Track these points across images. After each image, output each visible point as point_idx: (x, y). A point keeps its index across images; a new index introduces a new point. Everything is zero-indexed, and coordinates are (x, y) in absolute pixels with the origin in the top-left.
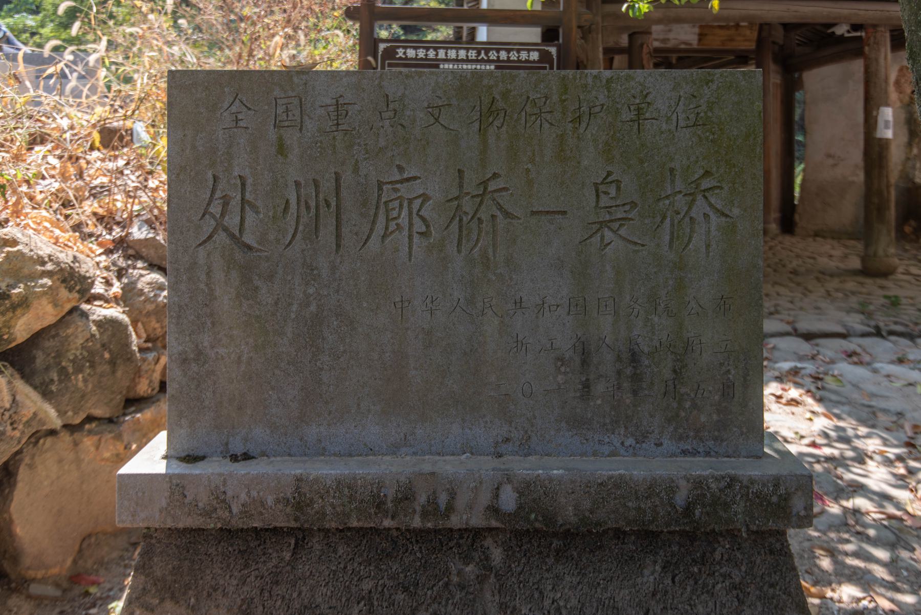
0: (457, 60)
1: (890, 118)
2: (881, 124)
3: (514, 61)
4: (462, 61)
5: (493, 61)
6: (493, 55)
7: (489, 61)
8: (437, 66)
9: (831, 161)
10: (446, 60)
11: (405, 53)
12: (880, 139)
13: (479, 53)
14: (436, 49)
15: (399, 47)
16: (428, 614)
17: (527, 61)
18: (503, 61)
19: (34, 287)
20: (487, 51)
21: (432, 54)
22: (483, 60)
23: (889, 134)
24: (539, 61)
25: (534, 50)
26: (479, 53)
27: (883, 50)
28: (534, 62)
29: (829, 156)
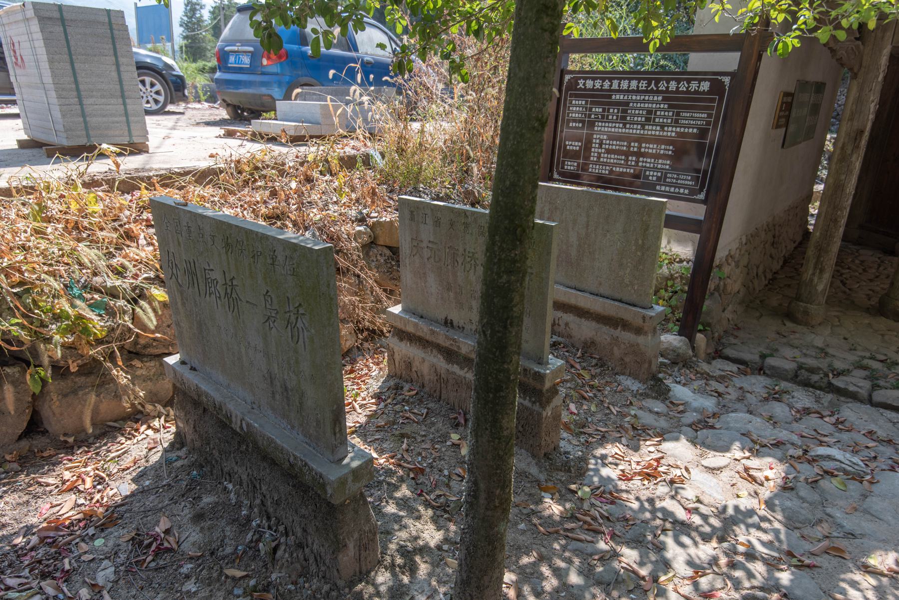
0: (628, 91)
3: (683, 92)
4: (633, 91)
7: (658, 92)
8: (610, 97)
10: (619, 91)
11: (584, 84)
13: (649, 84)
14: (611, 80)
15: (580, 78)
17: (696, 92)
18: (672, 92)
22: (652, 91)
25: (705, 80)
26: (649, 84)
28: (704, 93)
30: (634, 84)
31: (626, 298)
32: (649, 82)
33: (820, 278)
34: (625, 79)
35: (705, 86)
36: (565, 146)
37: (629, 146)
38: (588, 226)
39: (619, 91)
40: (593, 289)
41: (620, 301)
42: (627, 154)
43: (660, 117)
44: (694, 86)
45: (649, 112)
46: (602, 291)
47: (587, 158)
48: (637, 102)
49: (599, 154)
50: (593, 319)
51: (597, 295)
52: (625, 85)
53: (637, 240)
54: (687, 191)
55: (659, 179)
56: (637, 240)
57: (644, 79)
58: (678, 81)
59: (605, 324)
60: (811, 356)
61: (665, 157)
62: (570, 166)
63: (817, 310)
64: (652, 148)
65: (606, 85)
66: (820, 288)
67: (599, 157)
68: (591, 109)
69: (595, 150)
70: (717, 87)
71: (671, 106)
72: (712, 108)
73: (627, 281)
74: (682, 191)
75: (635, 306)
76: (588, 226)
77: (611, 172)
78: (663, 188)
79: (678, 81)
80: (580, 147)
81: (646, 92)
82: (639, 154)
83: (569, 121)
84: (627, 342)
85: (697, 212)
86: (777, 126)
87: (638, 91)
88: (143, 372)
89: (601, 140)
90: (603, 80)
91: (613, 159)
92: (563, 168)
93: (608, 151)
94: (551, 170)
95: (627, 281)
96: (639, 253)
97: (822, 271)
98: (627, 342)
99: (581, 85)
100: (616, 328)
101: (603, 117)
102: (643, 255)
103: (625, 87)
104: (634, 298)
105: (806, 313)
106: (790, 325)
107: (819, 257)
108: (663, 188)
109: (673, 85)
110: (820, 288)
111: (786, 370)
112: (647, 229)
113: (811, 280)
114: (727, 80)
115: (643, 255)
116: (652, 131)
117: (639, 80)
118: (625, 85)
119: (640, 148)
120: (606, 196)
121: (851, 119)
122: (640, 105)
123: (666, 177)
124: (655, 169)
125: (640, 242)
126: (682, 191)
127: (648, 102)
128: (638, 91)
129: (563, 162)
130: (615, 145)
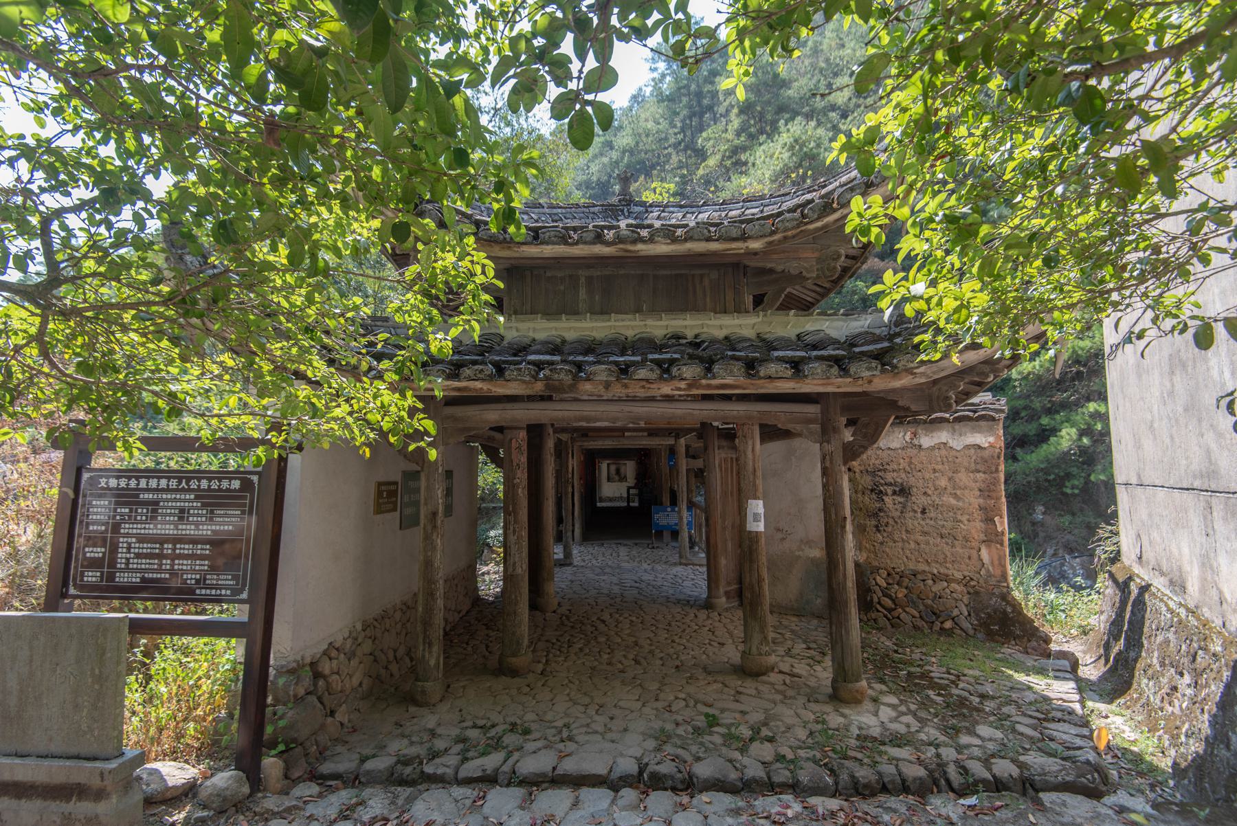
0: (157, 490)
1: (761, 510)
2: (750, 518)
3: (214, 490)
4: (163, 490)
5: (193, 490)
6: (194, 484)
7: (189, 490)
8: (137, 496)
9: (780, 535)
10: (148, 490)
11: (107, 483)
12: (750, 532)
13: (180, 482)
14: (137, 478)
15: (101, 477)
16: (526, 817)
17: (228, 490)
18: (204, 490)
19: (369, 445)
20: (188, 480)
21: (133, 483)
22: (183, 490)
23: (760, 527)
24: (240, 490)
25: (235, 478)
26: (180, 482)
27: (750, 443)
28: (235, 490)
29: (778, 530)
30: (163, 483)
31: (84, 751)
32: (180, 480)
33: (430, 653)
34: (153, 477)
35: (236, 484)
36: (85, 553)
37: (162, 549)
38: (31, 661)
39: (148, 490)
40: (42, 749)
41: (78, 757)
42: (161, 556)
43: (193, 515)
44: (225, 484)
45: (182, 511)
46: (54, 748)
47: (112, 564)
48: (168, 500)
49: (128, 559)
50: (39, 796)
51: (47, 756)
52: (153, 483)
53: (93, 669)
54: (228, 592)
55: (198, 582)
56: (93, 669)
57: (174, 478)
58: (210, 479)
59: (54, 798)
60: (961, 629)
61: (202, 557)
62: (91, 577)
63: (433, 687)
64: (187, 549)
65: (133, 483)
66: (432, 662)
67: (127, 564)
68: (115, 510)
69: (122, 555)
70: (247, 485)
71: (204, 505)
72: (244, 505)
73: (84, 727)
74: (223, 592)
75: (95, 759)
76: (31, 661)
77: (143, 580)
78: (203, 592)
79: (210, 479)
80: (104, 553)
81: (177, 490)
82: (174, 557)
83: (88, 524)
84: (82, 817)
85: (238, 613)
86: (379, 510)
87: (168, 490)
88: (903, 753)
89: (129, 544)
90: (129, 478)
91: (144, 563)
92: (82, 580)
93: (138, 556)
94: (65, 584)
95: (84, 727)
96: (97, 687)
97: (430, 645)
98: (82, 817)
99: (103, 484)
100: (68, 800)
101: (130, 517)
102: (101, 686)
103: (154, 486)
104: (94, 749)
105: (423, 692)
106: (412, 709)
107: (425, 631)
108: (203, 592)
109: (204, 484)
110: (432, 662)
111: (380, 771)
112: (103, 654)
113: (423, 656)
114: (255, 478)
115: (101, 686)
116: (189, 530)
117: (169, 478)
118: (153, 483)
119: (174, 549)
120: (54, 619)
121: (426, 504)
122: (171, 502)
123: (205, 579)
124: (194, 571)
125: (97, 671)
126: (223, 592)
127: (180, 500)
128: (168, 490)
129: (83, 573)
130: (146, 548)
